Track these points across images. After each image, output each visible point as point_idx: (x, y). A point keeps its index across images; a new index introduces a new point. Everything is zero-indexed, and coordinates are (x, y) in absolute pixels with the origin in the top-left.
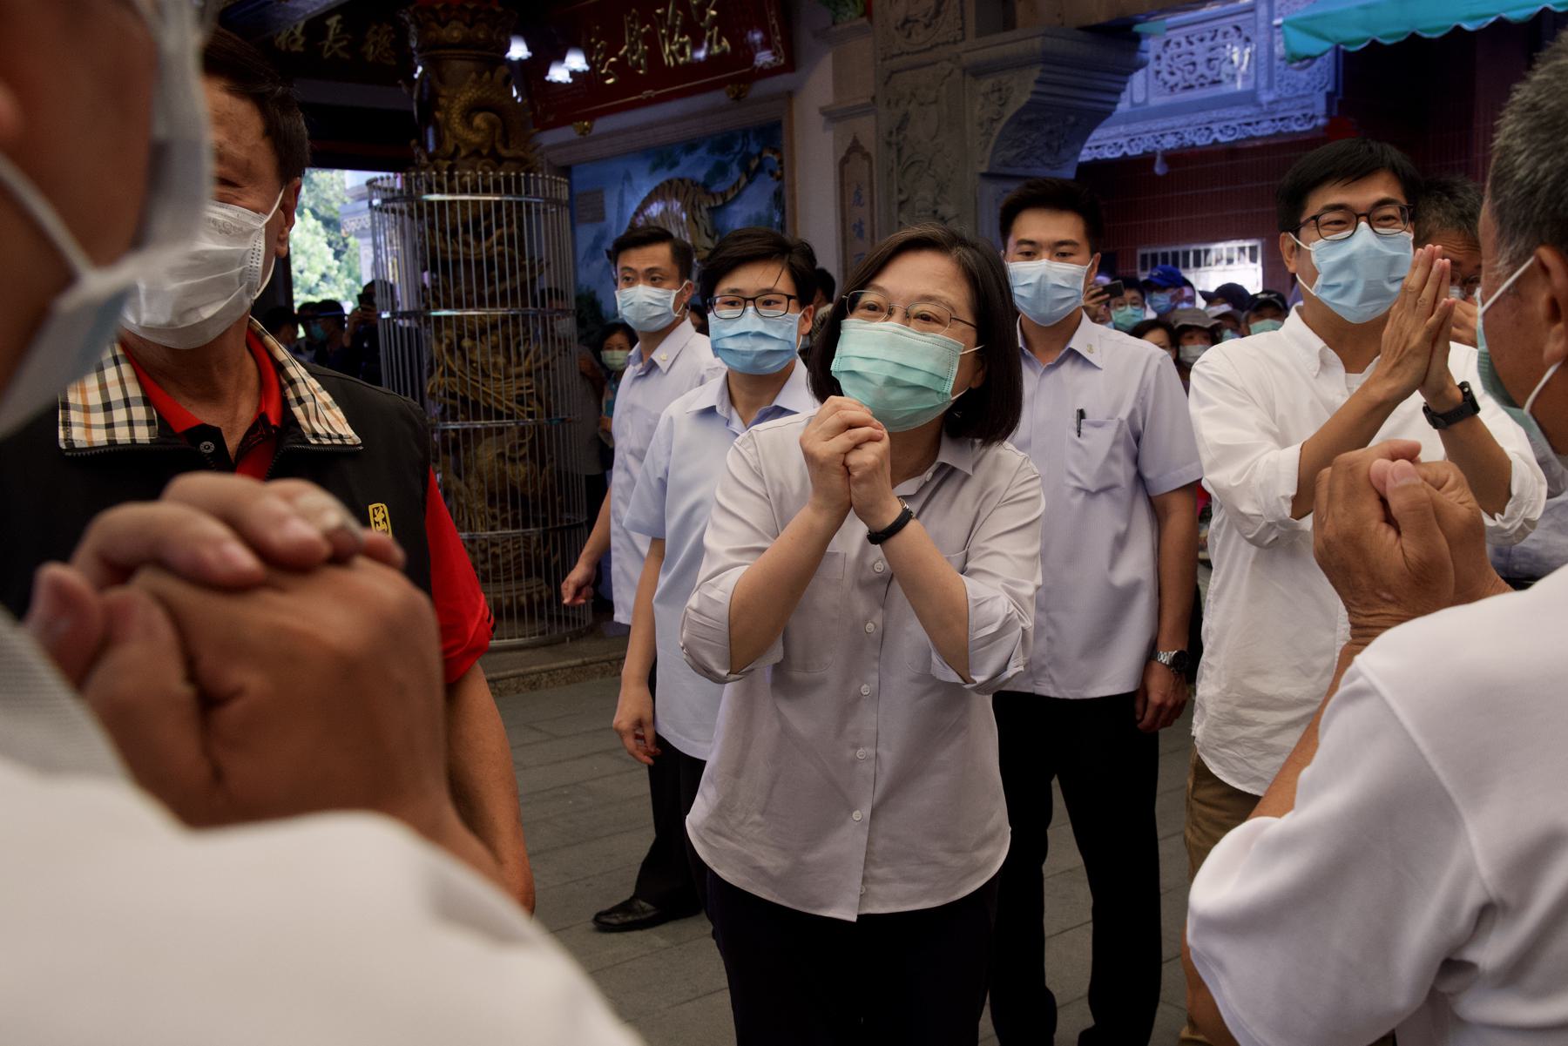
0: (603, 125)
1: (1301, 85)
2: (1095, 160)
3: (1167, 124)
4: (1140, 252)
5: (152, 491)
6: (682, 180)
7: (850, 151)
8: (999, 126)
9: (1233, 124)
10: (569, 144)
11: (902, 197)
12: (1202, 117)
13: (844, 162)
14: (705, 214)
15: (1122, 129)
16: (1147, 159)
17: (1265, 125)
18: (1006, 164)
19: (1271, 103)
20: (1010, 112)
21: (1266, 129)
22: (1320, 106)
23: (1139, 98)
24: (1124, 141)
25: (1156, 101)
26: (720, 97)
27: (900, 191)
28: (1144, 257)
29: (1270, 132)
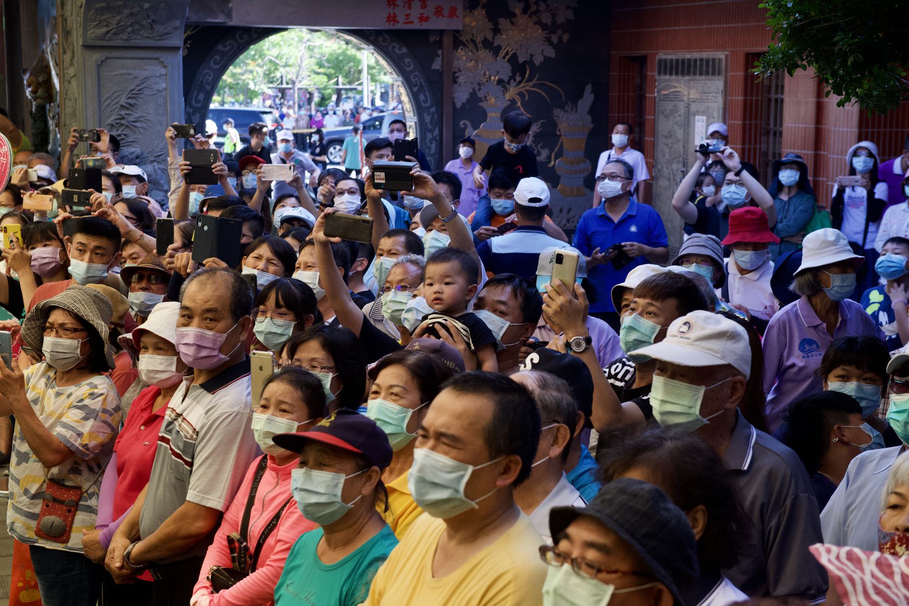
18: (102, 37)
28: (660, 61)
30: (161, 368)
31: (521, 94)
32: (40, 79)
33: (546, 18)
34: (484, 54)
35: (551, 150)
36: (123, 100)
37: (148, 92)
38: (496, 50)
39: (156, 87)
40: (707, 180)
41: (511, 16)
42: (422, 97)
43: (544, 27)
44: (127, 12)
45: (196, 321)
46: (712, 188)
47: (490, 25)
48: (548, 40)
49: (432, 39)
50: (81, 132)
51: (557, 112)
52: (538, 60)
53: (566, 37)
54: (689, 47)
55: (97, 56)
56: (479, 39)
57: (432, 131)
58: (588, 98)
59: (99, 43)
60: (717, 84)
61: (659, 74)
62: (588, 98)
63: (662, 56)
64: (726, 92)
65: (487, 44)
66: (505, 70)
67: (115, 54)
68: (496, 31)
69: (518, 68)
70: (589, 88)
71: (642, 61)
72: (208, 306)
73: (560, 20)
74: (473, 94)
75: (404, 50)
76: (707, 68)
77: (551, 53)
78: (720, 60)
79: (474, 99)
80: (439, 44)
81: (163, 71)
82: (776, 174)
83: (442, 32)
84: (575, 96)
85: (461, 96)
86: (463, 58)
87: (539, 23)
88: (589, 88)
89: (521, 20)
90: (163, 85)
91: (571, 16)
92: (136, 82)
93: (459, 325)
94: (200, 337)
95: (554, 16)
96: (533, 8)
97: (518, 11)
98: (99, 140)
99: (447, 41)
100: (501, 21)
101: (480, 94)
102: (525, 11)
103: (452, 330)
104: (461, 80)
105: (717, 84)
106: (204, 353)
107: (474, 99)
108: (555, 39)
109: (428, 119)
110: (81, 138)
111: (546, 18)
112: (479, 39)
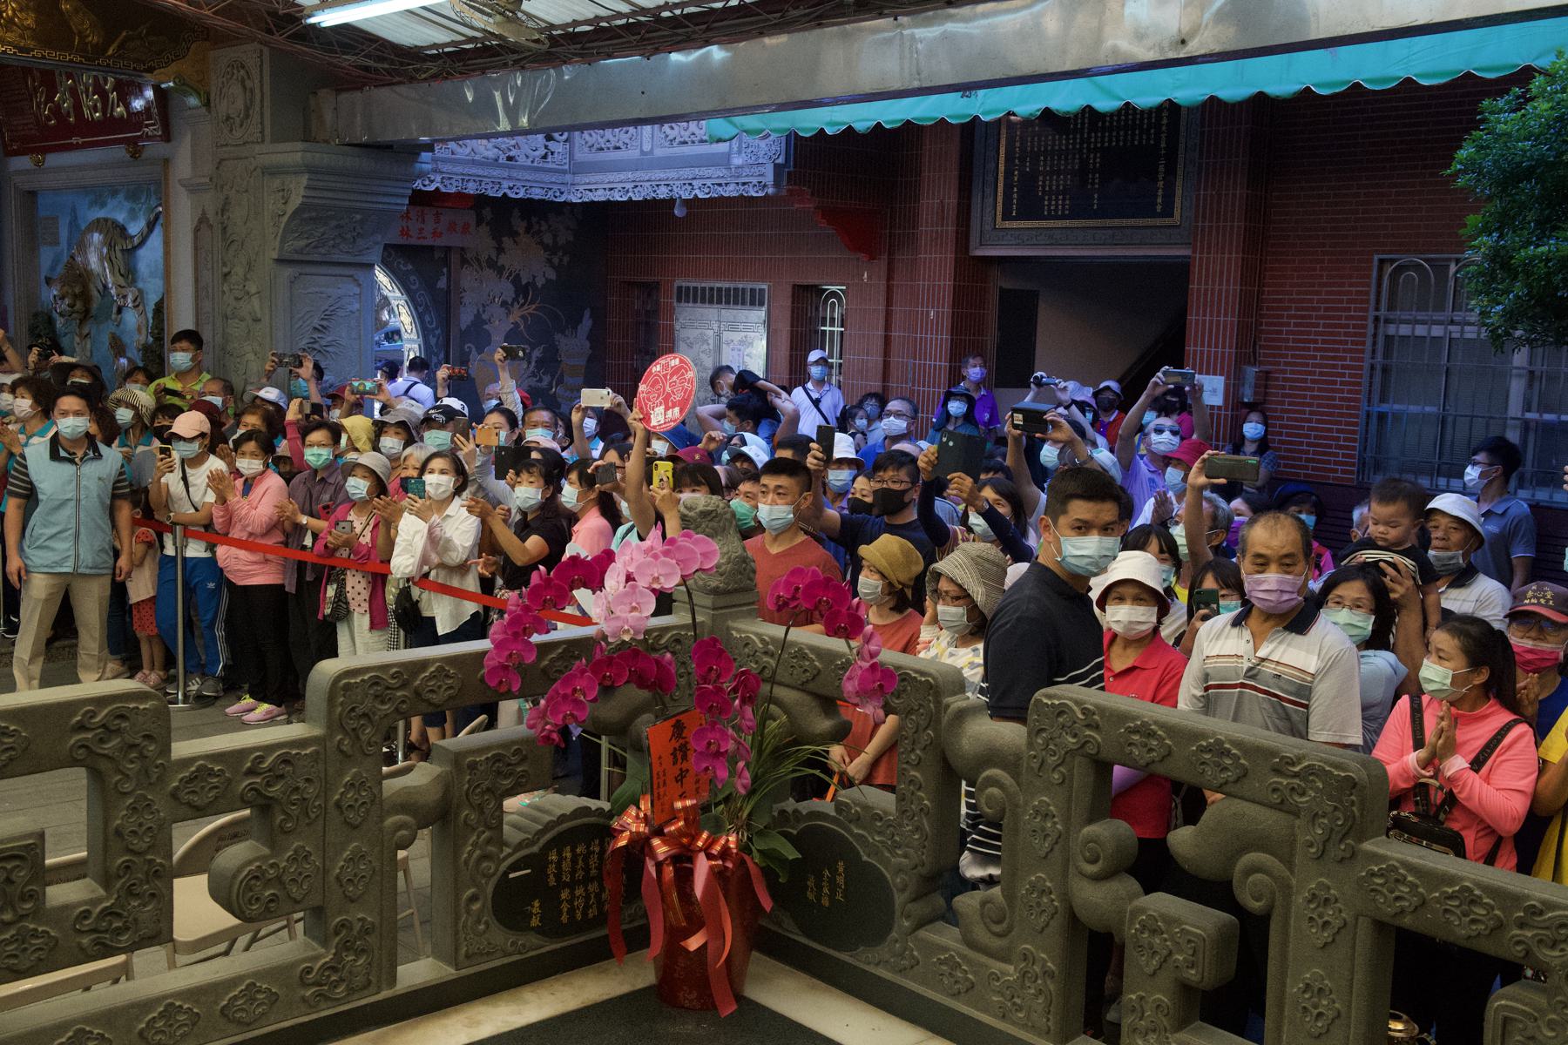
0: (53, 160)
1: (761, 154)
2: (609, 202)
3: (662, 175)
4: (679, 282)
5: (591, 337)
6: (106, 220)
7: (200, 221)
8: (285, 219)
9: (709, 183)
10: (28, 172)
11: (226, 270)
12: (687, 173)
13: (197, 230)
14: (119, 254)
15: (630, 175)
16: (670, 202)
17: (731, 187)
18: (299, 251)
19: (738, 167)
20: (291, 208)
21: (731, 191)
22: (769, 178)
23: (647, 148)
24: (629, 186)
25: (658, 152)
26: (120, 152)
27: (224, 264)
28: (680, 288)
29: (735, 194)
30: (1142, 619)
31: (522, 317)
32: (77, 290)
33: (548, 239)
34: (489, 273)
35: (553, 377)
36: (316, 322)
37: (341, 313)
38: (500, 270)
39: (350, 308)
40: (861, 413)
41: (514, 234)
42: (427, 318)
43: (546, 248)
44: (333, 223)
45: (1273, 567)
46: (865, 422)
47: (494, 244)
48: (549, 261)
49: (437, 255)
50: (281, 356)
51: (558, 336)
52: (540, 282)
53: (566, 259)
54: (716, 275)
55: (288, 272)
56: (483, 257)
57: (437, 355)
58: (587, 323)
59: (296, 257)
60: (760, 314)
61: (679, 300)
62: (587, 323)
63: (679, 282)
64: (769, 323)
65: (492, 264)
66: (508, 291)
67: (309, 269)
68: (500, 250)
69: (523, 290)
70: (587, 313)
71: (651, 289)
72: (1285, 551)
73: (561, 241)
74: (478, 316)
75: (410, 267)
76: (755, 300)
77: (552, 275)
78: (762, 291)
79: (479, 322)
80: (446, 262)
81: (357, 290)
82: (945, 404)
83: (448, 249)
84: (575, 322)
85: (466, 318)
86: (468, 278)
87: (541, 243)
88: (587, 313)
89: (524, 239)
90: (357, 306)
91: (571, 239)
92: (331, 301)
93: (1408, 562)
94: (1280, 582)
95: (555, 237)
96: (536, 227)
97: (521, 231)
98: (301, 365)
99: (455, 258)
100: (505, 239)
101: (485, 317)
102: (528, 230)
103: (1401, 567)
104: (466, 300)
105: (760, 314)
106: (1286, 597)
107: (479, 322)
108: (556, 261)
109: (433, 341)
110: (280, 364)
111: (548, 239)
112: (483, 257)
